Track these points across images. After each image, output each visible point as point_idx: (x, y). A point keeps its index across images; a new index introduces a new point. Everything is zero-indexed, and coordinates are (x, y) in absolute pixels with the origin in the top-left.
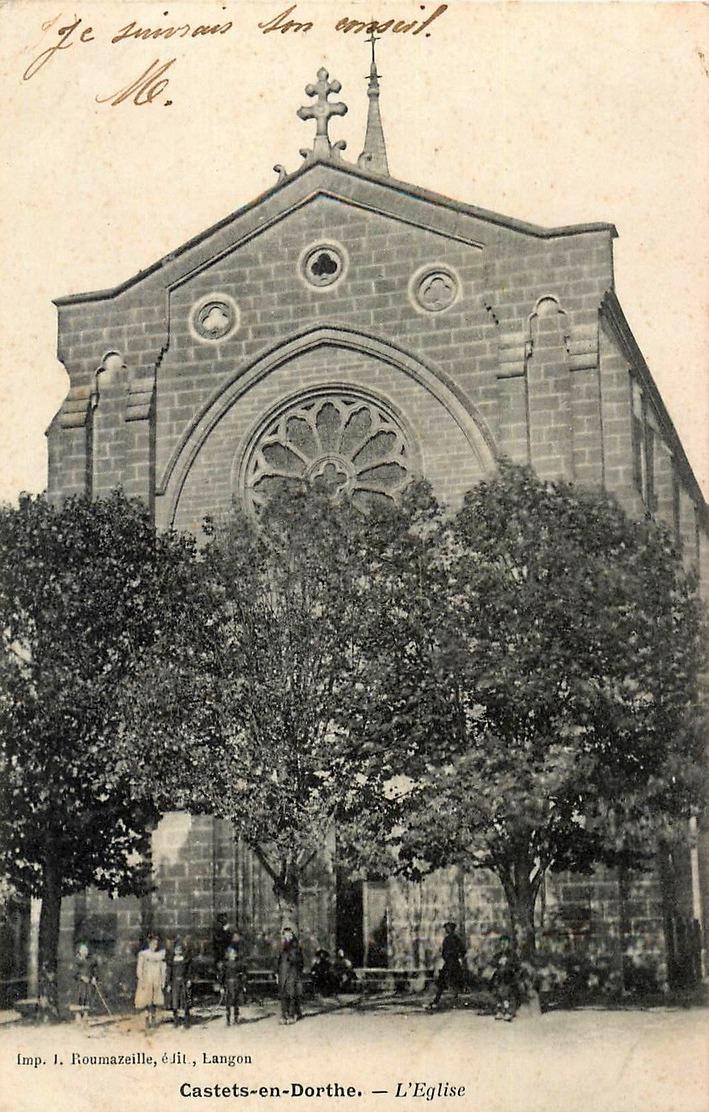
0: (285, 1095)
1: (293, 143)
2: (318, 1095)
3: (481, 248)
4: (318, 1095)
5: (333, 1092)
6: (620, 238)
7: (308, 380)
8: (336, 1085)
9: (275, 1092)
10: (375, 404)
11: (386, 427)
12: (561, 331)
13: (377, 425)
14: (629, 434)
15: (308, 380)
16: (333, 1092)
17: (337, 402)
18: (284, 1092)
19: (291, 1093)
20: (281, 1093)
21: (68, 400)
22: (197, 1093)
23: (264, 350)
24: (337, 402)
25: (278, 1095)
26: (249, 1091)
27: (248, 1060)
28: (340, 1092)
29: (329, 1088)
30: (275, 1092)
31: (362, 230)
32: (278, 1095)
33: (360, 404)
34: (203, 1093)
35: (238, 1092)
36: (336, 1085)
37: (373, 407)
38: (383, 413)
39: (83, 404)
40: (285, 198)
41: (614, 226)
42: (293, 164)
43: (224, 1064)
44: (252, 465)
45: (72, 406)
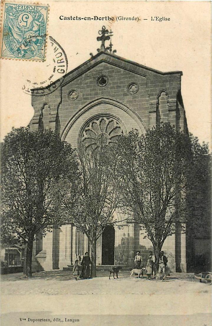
0: (92, 20)
1: (95, 46)
2: (103, 20)
3: (145, 77)
4: (103, 20)
5: (107, 19)
6: (183, 76)
7: (98, 112)
8: (108, 17)
9: (89, 19)
10: (115, 119)
11: (118, 125)
12: (166, 100)
13: (115, 125)
14: (183, 120)
15: (98, 112)
16: (107, 19)
17: (105, 118)
18: (92, 19)
19: (94, 19)
20: (91, 19)
21: (34, 116)
22: (66, 18)
23: (86, 104)
24: (105, 118)
25: (90, 20)
26: (81, 18)
27: (78, 320)
28: (109, 19)
29: (106, 17)
30: (89, 19)
31: (113, 71)
32: (90, 20)
33: (111, 119)
34: (67, 19)
35: (78, 19)
36: (108, 17)
37: (115, 120)
38: (117, 122)
39: (38, 117)
40: (93, 62)
41: (182, 72)
42: (95, 53)
43: (71, 322)
44: (82, 135)
45: (35, 118)
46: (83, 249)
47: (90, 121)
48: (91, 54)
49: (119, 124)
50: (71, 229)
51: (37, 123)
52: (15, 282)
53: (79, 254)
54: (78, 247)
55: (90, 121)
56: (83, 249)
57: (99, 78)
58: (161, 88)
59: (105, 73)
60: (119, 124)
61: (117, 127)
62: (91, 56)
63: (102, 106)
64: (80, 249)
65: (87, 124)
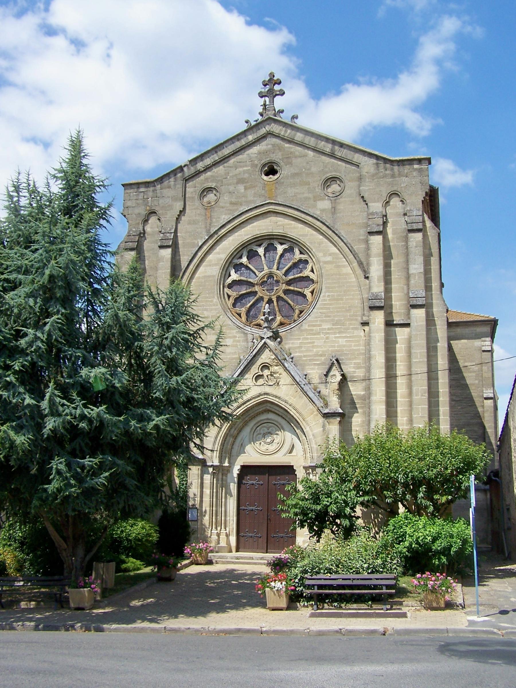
46: (226, 516)
47: (244, 248)
48: (247, 122)
49: (227, 294)
50: (200, 472)
51: (132, 249)
52: (188, 627)
53: (225, 528)
54: (214, 512)
55: (244, 248)
56: (226, 516)
57: (264, 166)
58: (390, 189)
59: (276, 157)
60: (227, 294)
61: (300, 261)
62: (247, 125)
63: (273, 219)
64: (219, 518)
65: (237, 253)
